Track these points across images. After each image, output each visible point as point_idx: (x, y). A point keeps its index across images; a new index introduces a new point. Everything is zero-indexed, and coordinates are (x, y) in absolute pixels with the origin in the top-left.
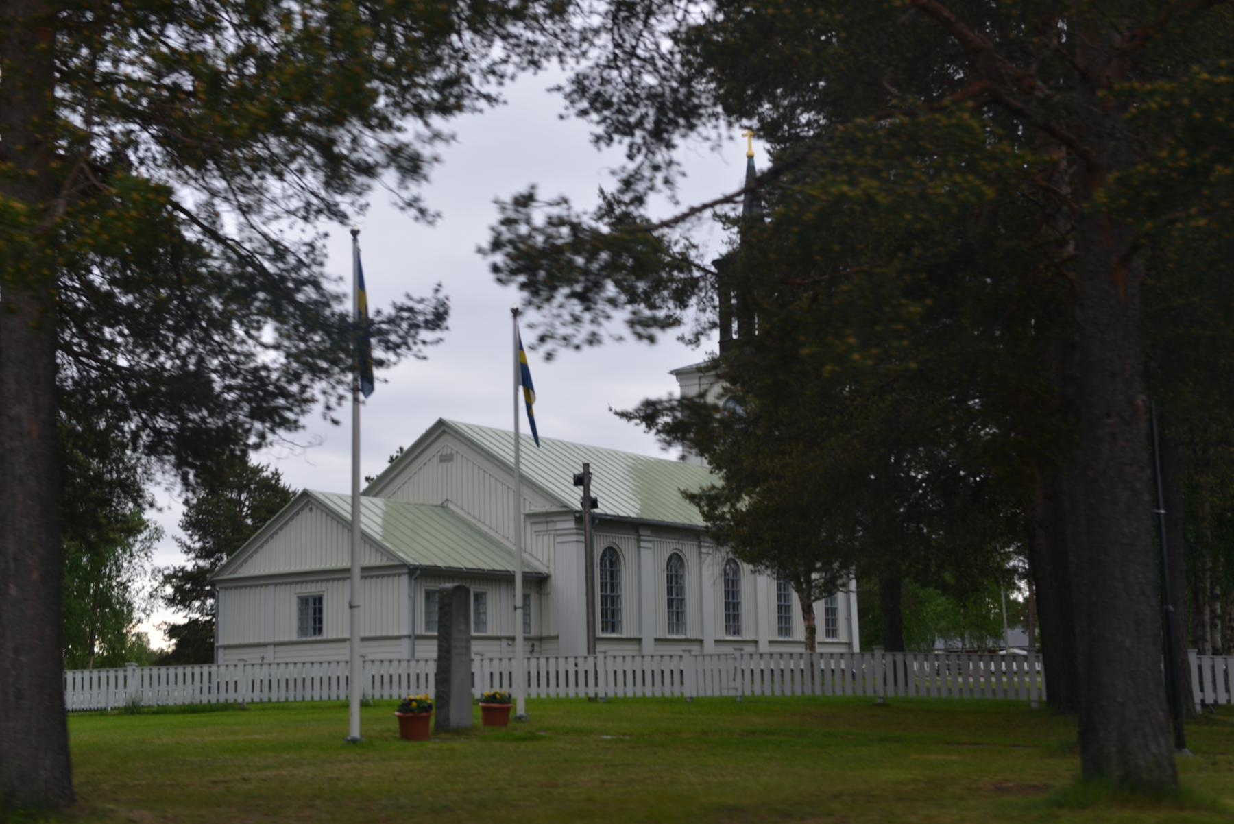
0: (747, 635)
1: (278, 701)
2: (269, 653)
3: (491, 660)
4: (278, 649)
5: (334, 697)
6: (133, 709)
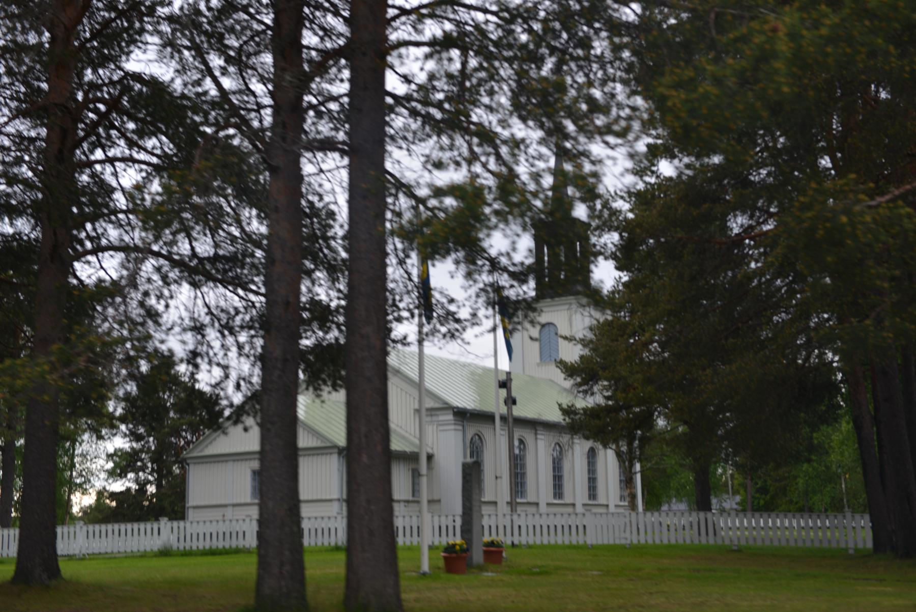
0: (568, 499)
2: (229, 512)
3: (205, 522)
4: (236, 508)
5: (319, 544)
6: (165, 553)
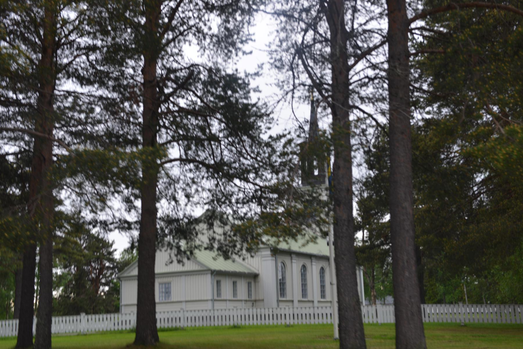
0: (310, 298)
1: (176, 327)
2: (183, 305)
4: (187, 303)
5: (205, 325)
